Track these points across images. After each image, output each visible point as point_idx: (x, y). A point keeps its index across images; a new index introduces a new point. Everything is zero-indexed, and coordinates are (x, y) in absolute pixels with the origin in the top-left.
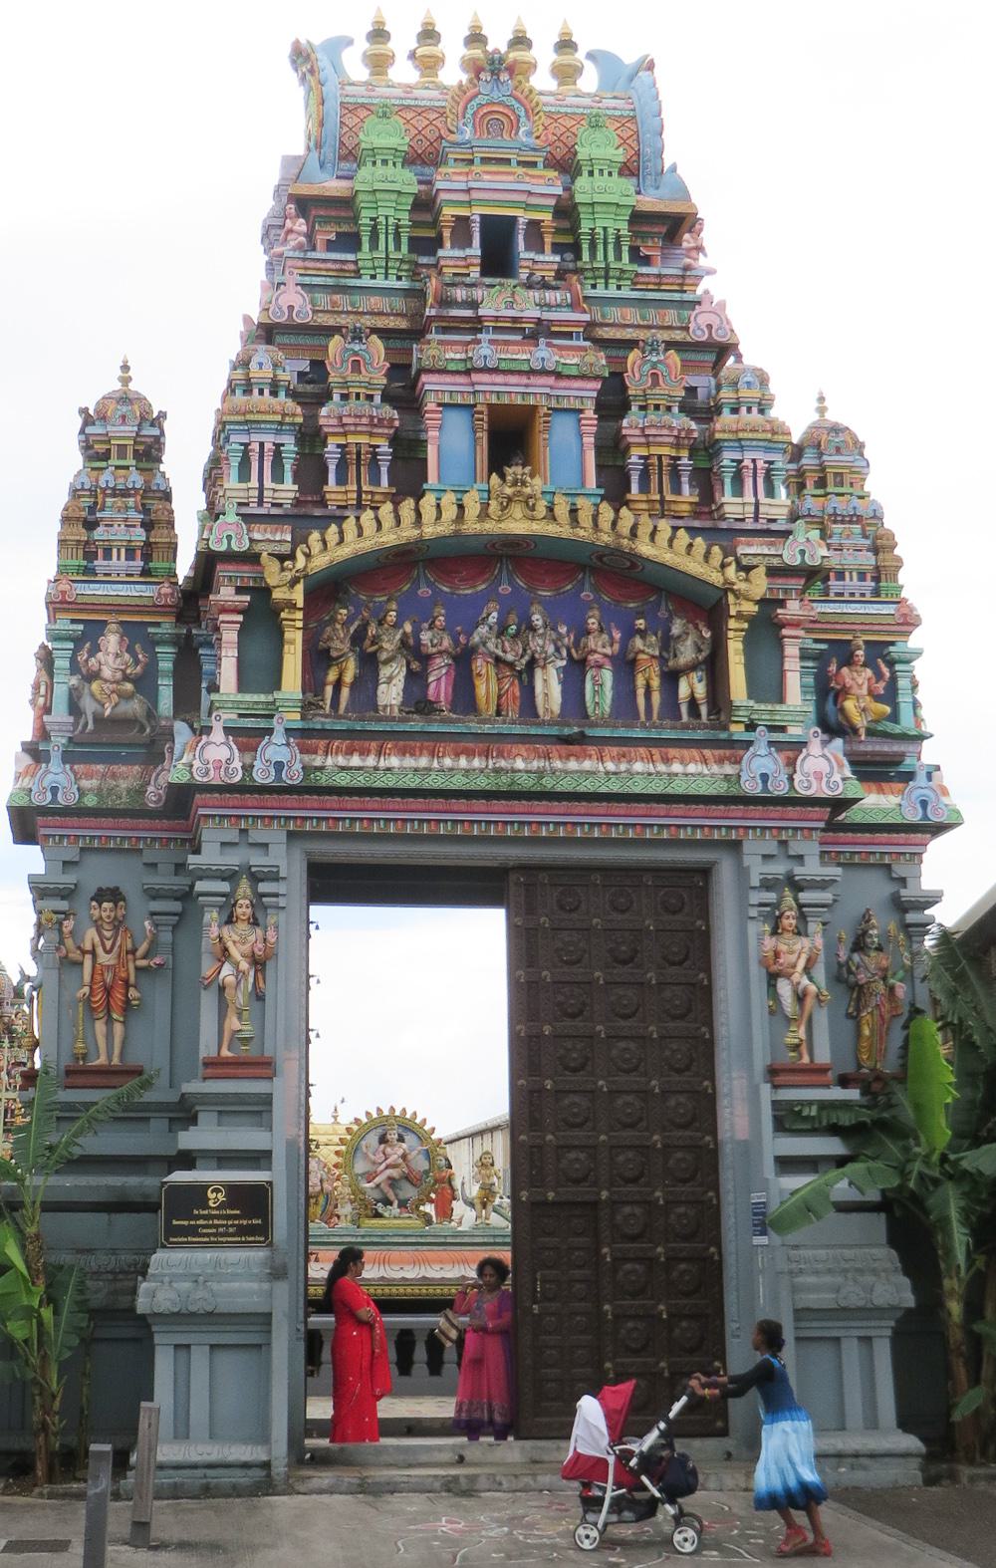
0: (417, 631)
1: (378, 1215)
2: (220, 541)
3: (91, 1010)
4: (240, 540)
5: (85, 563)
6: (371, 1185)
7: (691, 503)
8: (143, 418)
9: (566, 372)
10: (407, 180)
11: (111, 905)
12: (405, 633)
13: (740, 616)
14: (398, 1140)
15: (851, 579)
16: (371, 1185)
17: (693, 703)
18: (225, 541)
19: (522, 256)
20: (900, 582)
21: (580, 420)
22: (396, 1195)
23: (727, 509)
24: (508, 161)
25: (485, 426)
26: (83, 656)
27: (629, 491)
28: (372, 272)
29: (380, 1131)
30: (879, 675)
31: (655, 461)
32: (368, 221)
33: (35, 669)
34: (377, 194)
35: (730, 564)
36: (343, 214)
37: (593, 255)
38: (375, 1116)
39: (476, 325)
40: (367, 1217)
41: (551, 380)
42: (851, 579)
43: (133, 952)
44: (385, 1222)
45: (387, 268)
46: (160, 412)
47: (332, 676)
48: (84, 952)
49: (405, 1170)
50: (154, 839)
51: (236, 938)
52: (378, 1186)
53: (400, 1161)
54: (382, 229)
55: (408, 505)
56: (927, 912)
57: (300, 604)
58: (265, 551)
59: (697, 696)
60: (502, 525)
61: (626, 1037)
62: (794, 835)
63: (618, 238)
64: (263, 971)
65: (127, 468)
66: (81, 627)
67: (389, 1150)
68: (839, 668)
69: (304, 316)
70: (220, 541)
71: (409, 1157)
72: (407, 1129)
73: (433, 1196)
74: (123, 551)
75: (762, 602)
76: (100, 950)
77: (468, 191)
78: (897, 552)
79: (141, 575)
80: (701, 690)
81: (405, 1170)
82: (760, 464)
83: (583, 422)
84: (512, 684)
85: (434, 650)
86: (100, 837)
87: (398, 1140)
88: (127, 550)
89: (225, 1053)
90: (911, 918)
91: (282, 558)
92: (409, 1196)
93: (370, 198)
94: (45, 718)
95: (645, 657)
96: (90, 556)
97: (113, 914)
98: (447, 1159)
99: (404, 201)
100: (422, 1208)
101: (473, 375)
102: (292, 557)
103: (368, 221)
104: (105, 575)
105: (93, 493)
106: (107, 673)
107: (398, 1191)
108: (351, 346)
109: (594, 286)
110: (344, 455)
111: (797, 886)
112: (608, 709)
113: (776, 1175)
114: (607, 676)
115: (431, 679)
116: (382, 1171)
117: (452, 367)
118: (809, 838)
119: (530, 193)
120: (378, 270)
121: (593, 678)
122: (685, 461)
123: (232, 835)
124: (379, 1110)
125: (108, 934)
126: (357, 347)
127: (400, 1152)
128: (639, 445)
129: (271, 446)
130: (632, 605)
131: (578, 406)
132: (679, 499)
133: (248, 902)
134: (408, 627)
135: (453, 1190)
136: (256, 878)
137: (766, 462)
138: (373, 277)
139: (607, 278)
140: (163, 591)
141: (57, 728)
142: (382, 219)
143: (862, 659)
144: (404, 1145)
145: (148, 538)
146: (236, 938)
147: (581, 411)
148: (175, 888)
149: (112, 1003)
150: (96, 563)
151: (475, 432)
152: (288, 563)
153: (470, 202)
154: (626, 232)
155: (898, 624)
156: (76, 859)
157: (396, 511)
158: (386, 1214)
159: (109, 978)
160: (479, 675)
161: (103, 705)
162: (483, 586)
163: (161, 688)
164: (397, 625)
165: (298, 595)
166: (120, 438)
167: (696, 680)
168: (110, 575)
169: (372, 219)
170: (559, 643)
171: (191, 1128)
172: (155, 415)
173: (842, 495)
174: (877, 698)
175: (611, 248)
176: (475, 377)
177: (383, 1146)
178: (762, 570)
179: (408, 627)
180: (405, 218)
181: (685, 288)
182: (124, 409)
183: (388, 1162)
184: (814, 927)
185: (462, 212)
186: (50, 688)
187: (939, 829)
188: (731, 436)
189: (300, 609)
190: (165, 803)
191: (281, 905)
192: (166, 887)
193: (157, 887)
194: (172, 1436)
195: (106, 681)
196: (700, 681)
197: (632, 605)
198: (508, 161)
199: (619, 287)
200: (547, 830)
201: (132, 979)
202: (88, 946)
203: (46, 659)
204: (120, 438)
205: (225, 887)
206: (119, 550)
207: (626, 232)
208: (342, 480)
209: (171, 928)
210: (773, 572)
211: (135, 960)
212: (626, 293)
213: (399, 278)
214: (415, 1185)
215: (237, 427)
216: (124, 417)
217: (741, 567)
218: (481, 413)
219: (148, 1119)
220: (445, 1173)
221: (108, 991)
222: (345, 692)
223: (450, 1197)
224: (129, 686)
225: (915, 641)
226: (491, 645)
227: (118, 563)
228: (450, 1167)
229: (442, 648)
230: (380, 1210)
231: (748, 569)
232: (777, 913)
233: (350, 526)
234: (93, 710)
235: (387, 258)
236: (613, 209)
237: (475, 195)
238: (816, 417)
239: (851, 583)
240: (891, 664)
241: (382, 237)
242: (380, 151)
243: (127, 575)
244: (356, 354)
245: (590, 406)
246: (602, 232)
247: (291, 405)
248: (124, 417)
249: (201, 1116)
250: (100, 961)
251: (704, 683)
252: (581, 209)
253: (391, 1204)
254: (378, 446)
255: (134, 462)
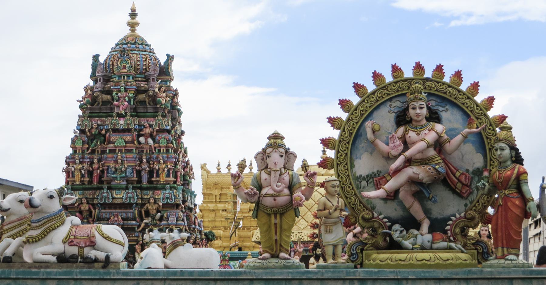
1: (395, 246)
6: (380, 193)
14: (429, 119)
16: (380, 193)
22: (427, 212)
29: (397, 104)
38: (389, 78)
40: (378, 248)
44: (402, 256)
49: (441, 168)
52: (393, 196)
53: (432, 152)
61: (226, 188)
67: (412, 135)
71: (449, 147)
72: (445, 100)
73: (490, 210)
81: (441, 168)
87: (429, 119)
92: (448, 212)
98: (513, 148)
100: (472, 232)
107: (429, 204)
116: (397, 171)
124: (358, 88)
127: (431, 137)
135: (525, 199)
144: (439, 127)
158: (407, 243)
177: (401, 130)
183: (408, 153)
214: (460, 195)
220: (512, 171)
223: (517, 211)
228: (518, 160)
230: (396, 236)
238: (127, 31)
253: (417, 226)
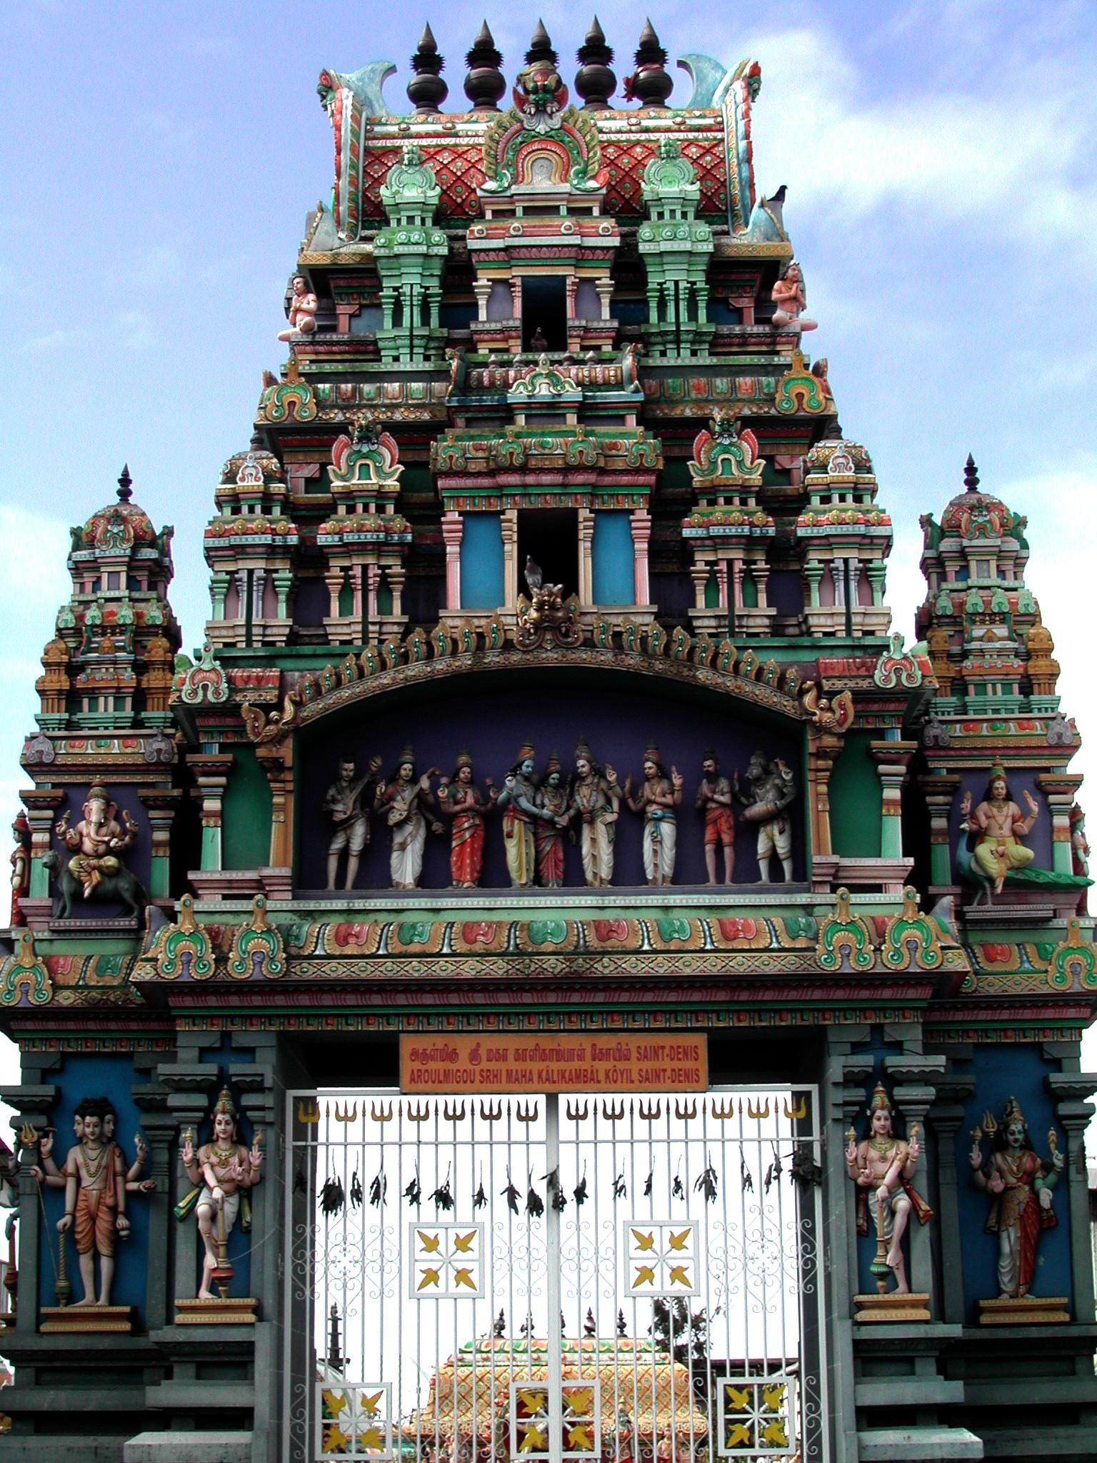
0: (435, 786)
2: (195, 692)
5: (66, 716)
7: (768, 617)
8: (138, 538)
10: (439, 241)
11: (95, 1119)
12: (421, 789)
13: (821, 754)
15: (995, 693)
17: (774, 858)
18: (200, 692)
19: (570, 323)
20: (1058, 693)
23: (812, 621)
25: (515, 538)
26: (62, 826)
27: (694, 606)
28: (395, 353)
30: (1025, 812)
31: (723, 566)
32: (391, 293)
33: (1026, 568)
35: (808, 691)
37: (662, 316)
39: (506, 413)
42: (995, 693)
43: (124, 1174)
46: (165, 527)
47: (337, 845)
51: (214, 1159)
54: (406, 302)
56: (1086, 1101)
57: (289, 762)
58: (246, 699)
59: (780, 851)
63: (693, 292)
64: (249, 1198)
65: (118, 600)
68: (975, 806)
69: (307, 413)
70: (195, 692)
75: (850, 735)
76: (83, 1173)
78: (1054, 655)
79: (132, 728)
80: (782, 844)
82: (854, 564)
83: (634, 525)
84: (554, 844)
85: (458, 808)
90: (1065, 1109)
91: (267, 708)
94: (23, 902)
95: (714, 805)
97: (97, 1130)
102: (279, 707)
103: (391, 293)
105: (77, 631)
106: (88, 846)
109: (663, 354)
110: (347, 578)
111: (893, 1080)
114: (667, 829)
115: (454, 844)
122: (762, 565)
129: (262, 574)
132: (754, 612)
133: (227, 1117)
134: (425, 783)
136: (238, 1090)
137: (860, 561)
138: (396, 359)
139: (678, 342)
142: (406, 289)
143: (1004, 792)
145: (139, 682)
146: (214, 1159)
147: (632, 512)
150: (79, 715)
152: (274, 714)
154: (703, 285)
156: (57, 1066)
160: (510, 836)
164: (414, 780)
165: (286, 752)
167: (776, 832)
168: (97, 728)
170: (610, 793)
171: (164, 1382)
172: (158, 532)
173: (988, 588)
174: (1021, 838)
175: (683, 305)
179: (425, 783)
180: (434, 286)
181: (779, 348)
184: (915, 1129)
186: (27, 862)
189: (289, 769)
190: (242, 981)
191: (268, 1120)
195: (88, 855)
196: (781, 833)
199: (694, 353)
201: (121, 1207)
203: (23, 831)
205: (201, 1100)
207: (703, 285)
208: (346, 610)
209: (165, 1145)
210: (858, 696)
211: (126, 1182)
212: (705, 359)
213: (427, 358)
217: (821, 693)
218: (510, 521)
219: (140, 1371)
222: (353, 864)
224: (111, 861)
225: (1074, 767)
226: (524, 803)
229: (467, 805)
231: (832, 695)
235: (412, 337)
236: (685, 258)
239: (995, 698)
240: (1042, 791)
241: (407, 310)
243: (116, 728)
246: (672, 287)
247: (285, 525)
249: (176, 1370)
250: (84, 1184)
251: (786, 835)
252: (648, 260)
254: (389, 567)
255: (126, 593)
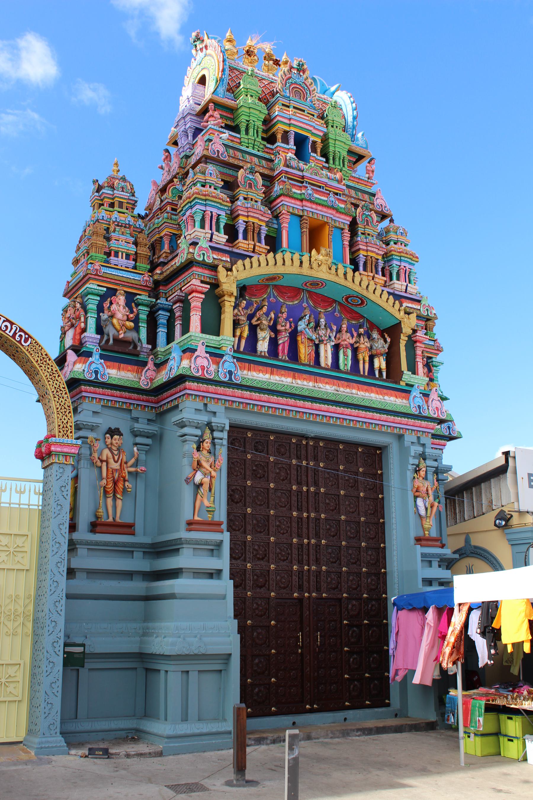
3: (106, 492)
4: (208, 257)
9: (340, 210)
18: (202, 256)
21: (342, 234)
24: (304, 111)
28: (247, 145)
34: (251, 110)
36: (229, 116)
41: (334, 212)
45: (254, 145)
48: (102, 461)
50: (138, 405)
55: (279, 256)
60: (318, 273)
62: (423, 434)
66: (105, 289)
74: (124, 254)
76: (111, 461)
77: (290, 119)
79: (132, 269)
80: (384, 366)
86: (112, 401)
88: (126, 254)
89: (196, 518)
93: (247, 110)
96: (108, 254)
99: (261, 116)
101: (304, 201)
104: (115, 265)
108: (248, 176)
112: (349, 369)
113: (423, 586)
117: (295, 196)
118: (427, 436)
119: (314, 128)
120: (250, 145)
121: (344, 352)
123: (201, 406)
125: (116, 452)
126: (251, 177)
128: (363, 250)
130: (354, 322)
131: (342, 227)
138: (247, 147)
140: (145, 278)
141: (91, 340)
148: (150, 431)
149: (117, 488)
151: (301, 229)
153: (290, 124)
155: (435, 350)
157: (274, 257)
159: (116, 475)
161: (118, 332)
162: (296, 302)
163: (141, 328)
166: (120, 198)
168: (117, 265)
169: (247, 121)
176: (304, 203)
178: (414, 315)
182: (123, 184)
185: (287, 129)
187: (451, 438)
188: (398, 254)
192: (146, 431)
193: (141, 430)
194: (197, 719)
197: (354, 322)
198: (304, 111)
200: (333, 420)
201: (127, 478)
202: (104, 458)
204: (120, 198)
206: (122, 254)
208: (245, 238)
215: (201, 202)
216: (123, 188)
221: (115, 483)
227: (122, 261)
232: (417, 469)
233: (255, 260)
234: (113, 333)
237: (292, 122)
242: (250, 91)
243: (126, 267)
244: (250, 180)
245: (347, 227)
248: (123, 188)
250: (110, 466)
